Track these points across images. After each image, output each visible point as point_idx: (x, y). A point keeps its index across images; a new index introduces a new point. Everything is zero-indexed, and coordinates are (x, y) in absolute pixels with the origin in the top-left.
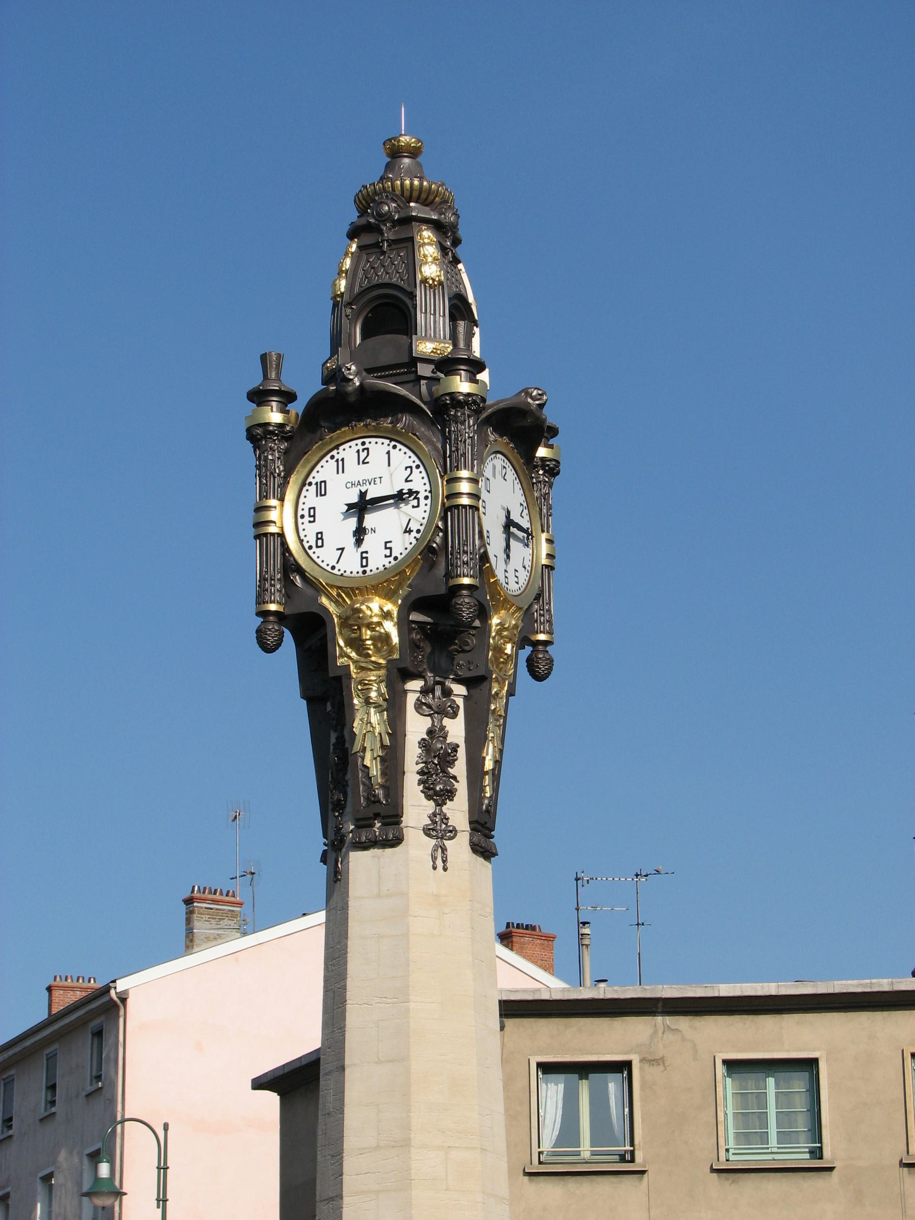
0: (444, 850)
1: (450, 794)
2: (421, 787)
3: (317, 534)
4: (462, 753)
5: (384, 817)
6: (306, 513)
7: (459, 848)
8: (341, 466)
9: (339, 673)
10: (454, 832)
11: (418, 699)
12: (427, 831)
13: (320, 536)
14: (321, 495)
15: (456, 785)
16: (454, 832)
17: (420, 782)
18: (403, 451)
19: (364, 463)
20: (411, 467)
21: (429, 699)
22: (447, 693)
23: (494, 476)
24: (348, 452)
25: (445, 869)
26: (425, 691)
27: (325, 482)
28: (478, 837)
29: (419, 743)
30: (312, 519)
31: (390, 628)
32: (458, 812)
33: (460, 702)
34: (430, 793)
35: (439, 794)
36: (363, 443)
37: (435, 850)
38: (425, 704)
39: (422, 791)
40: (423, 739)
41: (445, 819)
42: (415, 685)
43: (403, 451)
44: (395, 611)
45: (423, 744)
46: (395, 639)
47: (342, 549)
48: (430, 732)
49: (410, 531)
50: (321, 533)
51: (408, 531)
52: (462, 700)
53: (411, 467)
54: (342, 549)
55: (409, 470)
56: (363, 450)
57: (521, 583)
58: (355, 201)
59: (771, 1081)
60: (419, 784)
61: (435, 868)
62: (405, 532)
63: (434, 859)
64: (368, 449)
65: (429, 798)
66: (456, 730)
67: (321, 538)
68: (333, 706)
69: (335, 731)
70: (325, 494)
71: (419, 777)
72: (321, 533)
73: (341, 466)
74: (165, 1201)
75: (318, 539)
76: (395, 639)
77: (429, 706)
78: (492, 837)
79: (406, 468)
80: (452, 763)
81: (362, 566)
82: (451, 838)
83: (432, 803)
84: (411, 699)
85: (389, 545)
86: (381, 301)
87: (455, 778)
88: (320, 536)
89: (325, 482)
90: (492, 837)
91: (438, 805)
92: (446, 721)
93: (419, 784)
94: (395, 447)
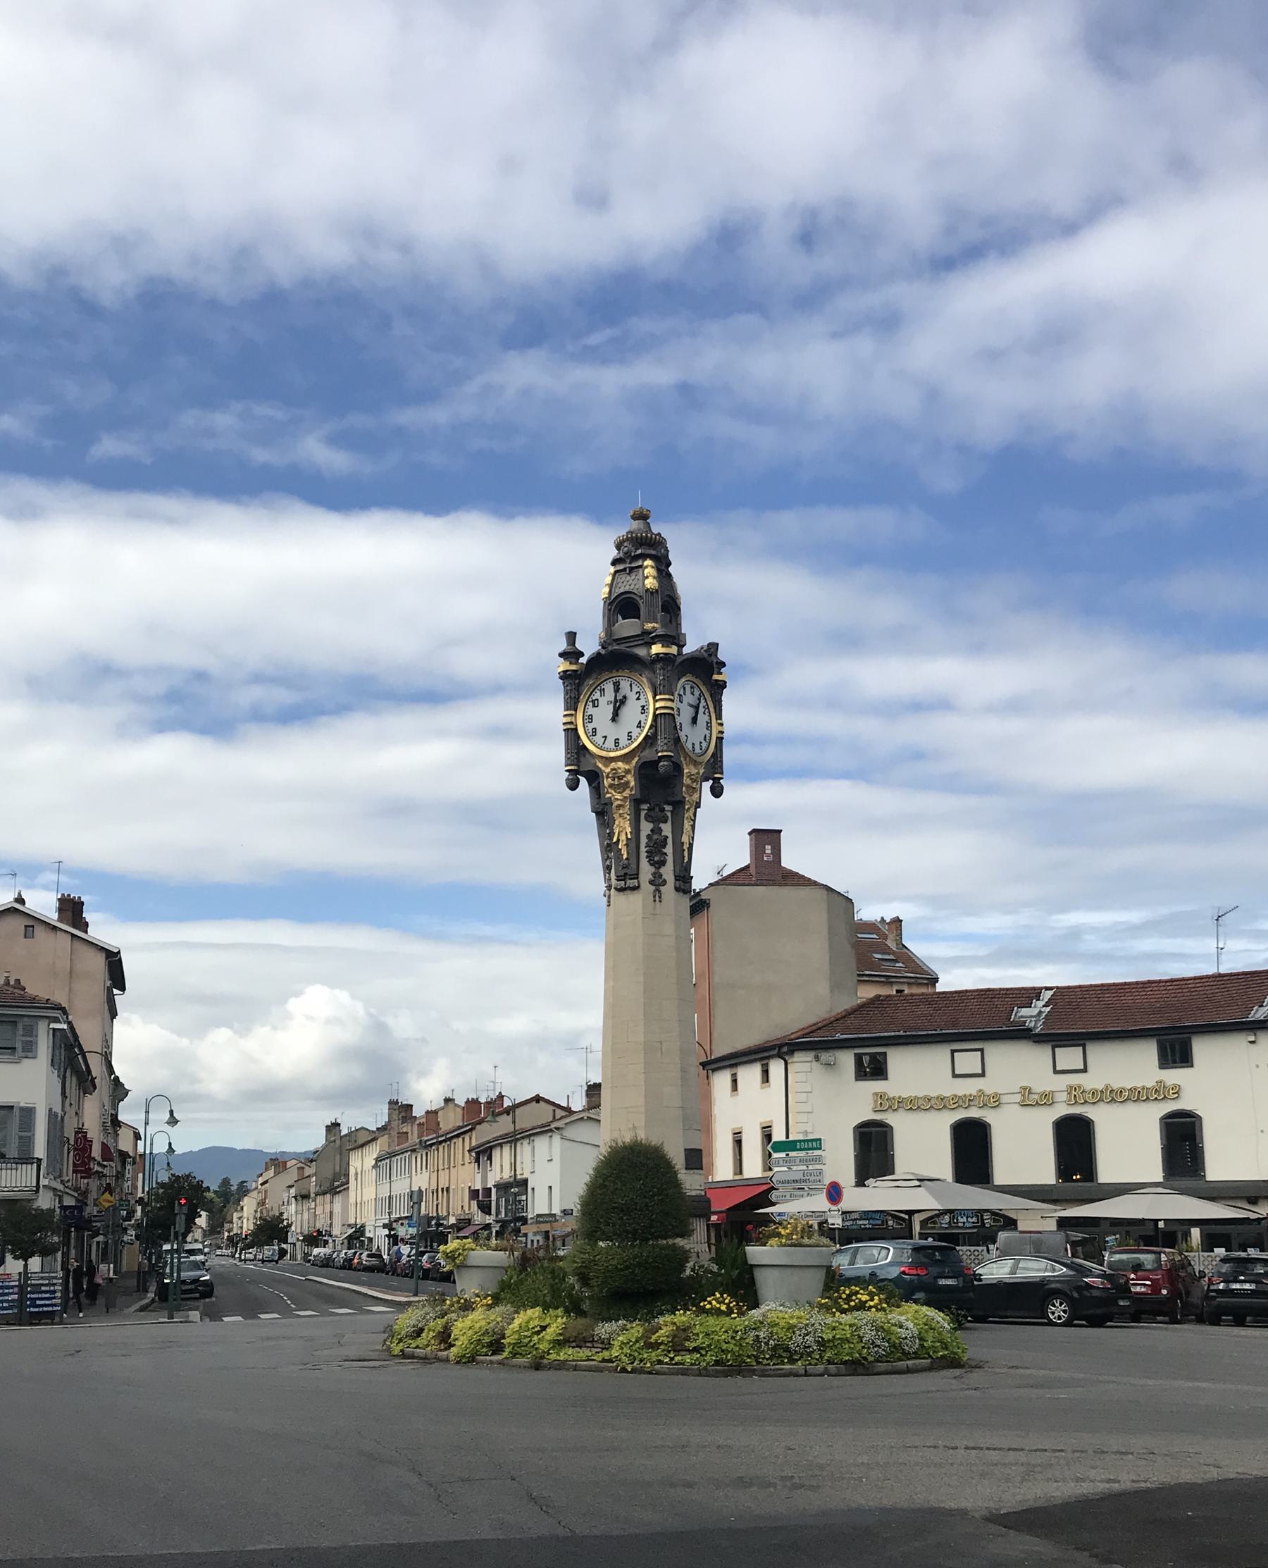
1: (663, 863)
4: (670, 841)
12: (651, 882)
16: (665, 882)
21: (652, 813)
22: (663, 810)
26: (649, 810)
32: (668, 872)
33: (669, 814)
34: (652, 863)
42: (645, 806)
45: (648, 837)
66: (667, 829)
84: (643, 814)
88: (594, 731)
92: (662, 825)
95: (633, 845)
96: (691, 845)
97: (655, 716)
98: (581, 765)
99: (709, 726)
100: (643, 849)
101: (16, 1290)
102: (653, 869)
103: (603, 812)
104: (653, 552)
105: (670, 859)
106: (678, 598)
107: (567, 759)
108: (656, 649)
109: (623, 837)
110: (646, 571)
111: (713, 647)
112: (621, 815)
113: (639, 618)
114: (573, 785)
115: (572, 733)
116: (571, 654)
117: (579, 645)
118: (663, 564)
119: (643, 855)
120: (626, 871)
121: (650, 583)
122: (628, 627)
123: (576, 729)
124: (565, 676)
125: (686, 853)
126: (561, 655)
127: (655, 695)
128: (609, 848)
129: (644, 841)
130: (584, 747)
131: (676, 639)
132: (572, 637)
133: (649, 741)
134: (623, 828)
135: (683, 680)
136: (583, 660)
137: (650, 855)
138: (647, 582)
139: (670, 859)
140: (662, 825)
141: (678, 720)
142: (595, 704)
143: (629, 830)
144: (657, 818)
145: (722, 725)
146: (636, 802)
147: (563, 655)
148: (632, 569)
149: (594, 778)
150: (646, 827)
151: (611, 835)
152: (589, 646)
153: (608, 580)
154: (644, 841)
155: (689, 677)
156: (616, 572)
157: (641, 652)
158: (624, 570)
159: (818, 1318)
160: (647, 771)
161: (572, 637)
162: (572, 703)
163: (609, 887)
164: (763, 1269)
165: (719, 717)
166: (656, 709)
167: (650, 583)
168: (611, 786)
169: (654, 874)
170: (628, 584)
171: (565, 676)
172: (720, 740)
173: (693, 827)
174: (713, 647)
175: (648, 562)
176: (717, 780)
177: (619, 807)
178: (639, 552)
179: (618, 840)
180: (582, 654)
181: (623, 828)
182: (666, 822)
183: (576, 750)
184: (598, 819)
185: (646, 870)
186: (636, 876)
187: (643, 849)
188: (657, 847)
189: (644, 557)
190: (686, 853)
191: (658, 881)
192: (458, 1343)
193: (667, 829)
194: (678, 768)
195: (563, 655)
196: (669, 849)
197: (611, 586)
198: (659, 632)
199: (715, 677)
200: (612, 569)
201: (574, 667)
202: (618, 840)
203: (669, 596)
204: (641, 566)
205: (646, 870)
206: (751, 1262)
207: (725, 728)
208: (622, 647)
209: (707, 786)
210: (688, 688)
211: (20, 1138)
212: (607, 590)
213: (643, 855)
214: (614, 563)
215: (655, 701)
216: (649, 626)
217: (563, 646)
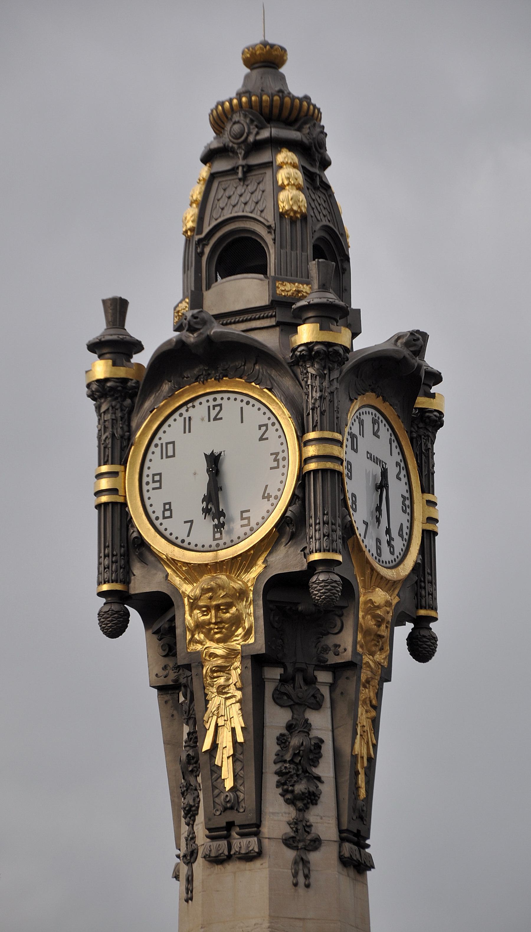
0: (305, 863)
1: (311, 799)
2: (280, 790)
3: (165, 504)
4: (327, 750)
5: (241, 826)
6: (150, 479)
7: (325, 861)
10: (316, 843)
11: (276, 689)
12: (289, 842)
13: (168, 507)
14: (167, 457)
15: (321, 786)
16: (316, 843)
17: (279, 784)
18: (256, 407)
19: (215, 419)
20: (266, 425)
21: (289, 688)
22: (311, 681)
23: (362, 433)
26: (283, 680)
27: (173, 443)
28: (348, 848)
29: (278, 739)
30: (157, 485)
32: (324, 820)
33: (325, 691)
36: (215, 399)
37: (295, 863)
38: (285, 694)
39: (281, 795)
41: (308, 827)
42: (274, 674)
43: (256, 407)
45: (282, 741)
47: (192, 522)
48: (290, 727)
49: (268, 497)
50: (169, 504)
52: (327, 688)
53: (266, 425)
54: (192, 522)
55: (264, 428)
56: (214, 406)
57: (397, 553)
58: (212, 111)
60: (278, 786)
61: (296, 885)
62: (264, 497)
63: (295, 875)
64: (220, 405)
67: (170, 510)
68: (185, 696)
69: (187, 724)
70: (174, 456)
72: (169, 504)
75: (165, 510)
77: (289, 697)
78: (368, 846)
79: (260, 427)
81: (215, 539)
82: (316, 849)
84: (269, 689)
85: (245, 515)
87: (319, 779)
88: (168, 507)
89: (173, 443)
90: (368, 846)
91: (299, 810)
93: (278, 786)
94: (248, 403)
95: (250, 754)
96: (372, 761)
97: (303, 478)
98: (133, 591)
99: (409, 507)
102: (291, 812)
103: (180, 689)
104: (293, 134)
105: (327, 790)
106: (344, 234)
107: (102, 569)
108: (306, 333)
109: (225, 740)
110: (282, 176)
111: (417, 341)
112: (222, 690)
113: (262, 269)
114: (114, 626)
115: (114, 516)
116: (117, 346)
117: (133, 328)
118: (313, 157)
119: (271, 780)
120: (230, 816)
121: (290, 199)
122: (245, 291)
123: (125, 504)
124: (99, 391)
125: (361, 780)
126: (93, 347)
127: (301, 430)
128: (191, 764)
129: (271, 747)
130: (141, 544)
131: (339, 313)
132: (117, 309)
133: (290, 527)
134: (226, 718)
135: (356, 405)
136: (143, 359)
137: (285, 781)
138: (282, 196)
141: (350, 487)
142: (169, 452)
143: (238, 723)
145: (432, 504)
146: (257, 663)
147: (97, 347)
148: (249, 169)
149: (159, 609)
150: (277, 718)
151: (195, 739)
152: (153, 330)
153: (197, 192)
154: (271, 747)
155: (370, 398)
156: (213, 177)
157: (269, 339)
158: (233, 171)
160: (284, 596)
161: (117, 309)
162: (116, 447)
163: (190, 857)
165: (428, 487)
166: (304, 461)
167: (290, 199)
168: (199, 626)
169: (295, 824)
170: (237, 203)
171: (99, 391)
172: (429, 536)
173: (375, 722)
174: (417, 341)
175: (284, 156)
176: (422, 624)
177: (222, 669)
178: (265, 134)
179: (215, 746)
180: (138, 347)
181: (226, 718)
182: (317, 706)
183: (122, 544)
184: (163, 704)
185: (277, 816)
186: (254, 829)
188: (299, 764)
189: (277, 144)
190: (361, 780)
191: (301, 840)
193: (320, 722)
194: (348, 590)
195: (97, 347)
196: (325, 769)
197: (203, 205)
198: (315, 298)
199: (422, 402)
200: (204, 171)
201: (121, 372)
202: (215, 746)
203: (326, 229)
204: (269, 165)
205: (277, 816)
207: (440, 512)
208: (236, 329)
209: (402, 633)
210: (368, 420)
212: (192, 212)
213: (271, 780)
214: (208, 158)
215: (303, 443)
216: (287, 289)
217: (98, 327)
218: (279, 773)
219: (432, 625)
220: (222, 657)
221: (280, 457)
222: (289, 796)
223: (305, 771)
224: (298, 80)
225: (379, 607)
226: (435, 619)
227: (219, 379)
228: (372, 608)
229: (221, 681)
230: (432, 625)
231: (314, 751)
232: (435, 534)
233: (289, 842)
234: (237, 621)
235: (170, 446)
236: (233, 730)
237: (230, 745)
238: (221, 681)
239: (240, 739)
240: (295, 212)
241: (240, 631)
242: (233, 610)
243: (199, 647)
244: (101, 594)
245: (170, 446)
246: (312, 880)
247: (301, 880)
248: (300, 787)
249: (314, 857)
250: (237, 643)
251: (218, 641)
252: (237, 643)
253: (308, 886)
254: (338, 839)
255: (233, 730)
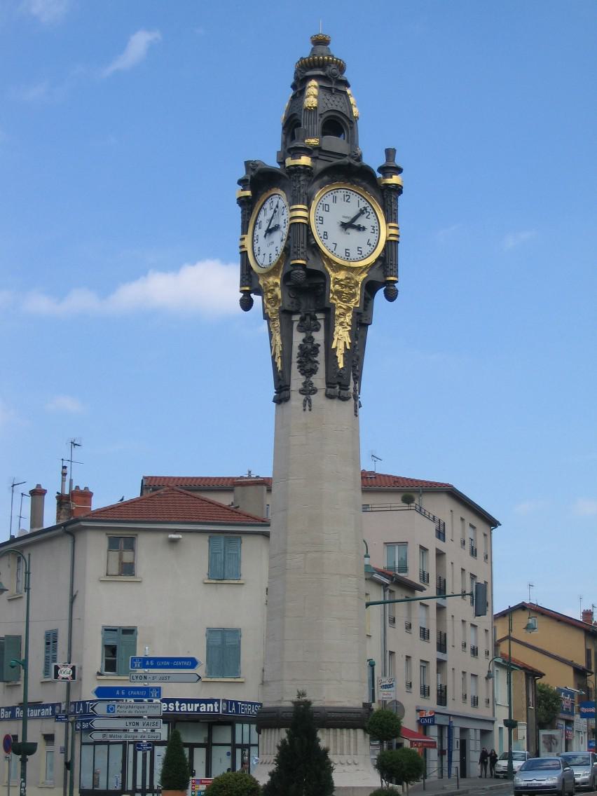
1: (313, 371)
2: (299, 370)
4: (322, 350)
8: (335, 200)
9: (328, 306)
12: (302, 392)
15: (318, 366)
16: (314, 391)
19: (347, 201)
22: (315, 319)
24: (340, 195)
25: (310, 410)
26: (302, 320)
31: (278, 291)
32: (319, 380)
33: (322, 323)
35: (308, 371)
37: (305, 401)
40: (301, 345)
42: (296, 318)
44: (278, 281)
45: (301, 347)
46: (280, 297)
49: (370, 245)
51: (282, 241)
52: (323, 321)
59: (397, 547)
61: (305, 410)
63: (305, 406)
65: (302, 374)
66: (319, 337)
71: (298, 364)
73: (335, 200)
74: (29, 589)
76: (280, 297)
80: (316, 354)
82: (314, 393)
83: (304, 377)
84: (295, 325)
86: (339, 115)
87: (317, 362)
91: (307, 377)
92: (315, 334)
100: (295, 359)
101: (216, 710)
102: (302, 379)
112: (341, 324)
119: (295, 366)
139: (321, 368)
140: (315, 334)
144: (308, 326)
147: (398, 189)
159: (395, 744)
164: (70, 545)
166: (308, 210)
169: (304, 384)
175: (314, 83)
182: (317, 330)
185: (297, 380)
187: (295, 359)
192: (431, 778)
193: (319, 337)
206: (80, 539)
211: (21, 593)
213: (295, 366)
218: (298, 362)
219: (395, 285)
220: (344, 309)
221: (375, 228)
222: (303, 372)
223: (310, 360)
224: (337, 50)
225: (342, 280)
226: (396, 282)
227: (267, 191)
228: (337, 282)
229: (342, 320)
230: (395, 285)
231: (315, 349)
232: (398, 242)
233: (302, 392)
234: (354, 295)
235: (327, 206)
236: (345, 343)
237: (343, 349)
238: (342, 320)
239: (348, 347)
240: (310, 107)
241: (354, 300)
242: (353, 290)
243: (334, 302)
244: (241, 291)
245: (327, 206)
246: (312, 408)
247: (307, 408)
248: (309, 366)
249: (312, 397)
250: (352, 305)
251: (344, 302)
252: (352, 305)
253: (310, 410)
254: (325, 387)
255: (345, 343)
